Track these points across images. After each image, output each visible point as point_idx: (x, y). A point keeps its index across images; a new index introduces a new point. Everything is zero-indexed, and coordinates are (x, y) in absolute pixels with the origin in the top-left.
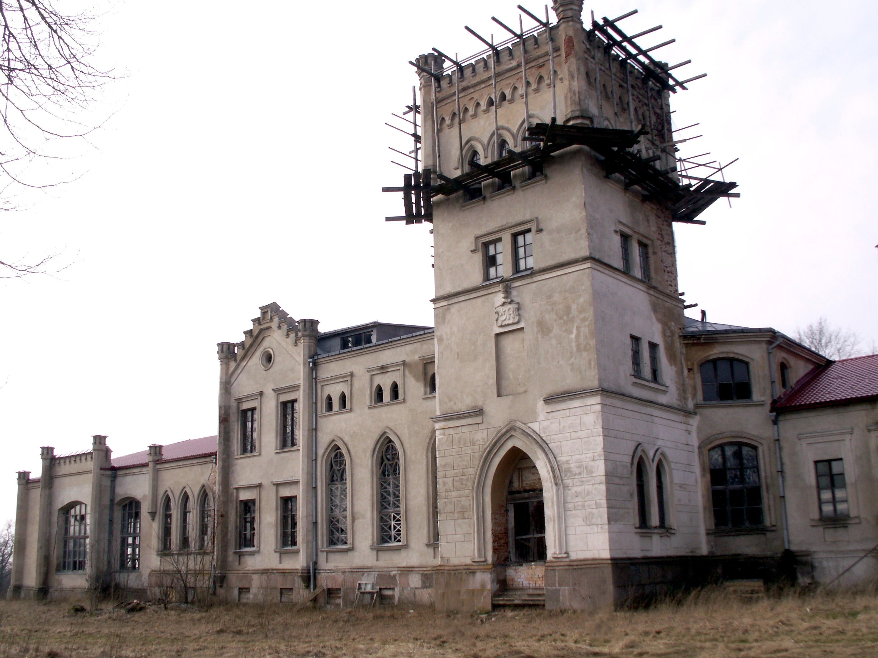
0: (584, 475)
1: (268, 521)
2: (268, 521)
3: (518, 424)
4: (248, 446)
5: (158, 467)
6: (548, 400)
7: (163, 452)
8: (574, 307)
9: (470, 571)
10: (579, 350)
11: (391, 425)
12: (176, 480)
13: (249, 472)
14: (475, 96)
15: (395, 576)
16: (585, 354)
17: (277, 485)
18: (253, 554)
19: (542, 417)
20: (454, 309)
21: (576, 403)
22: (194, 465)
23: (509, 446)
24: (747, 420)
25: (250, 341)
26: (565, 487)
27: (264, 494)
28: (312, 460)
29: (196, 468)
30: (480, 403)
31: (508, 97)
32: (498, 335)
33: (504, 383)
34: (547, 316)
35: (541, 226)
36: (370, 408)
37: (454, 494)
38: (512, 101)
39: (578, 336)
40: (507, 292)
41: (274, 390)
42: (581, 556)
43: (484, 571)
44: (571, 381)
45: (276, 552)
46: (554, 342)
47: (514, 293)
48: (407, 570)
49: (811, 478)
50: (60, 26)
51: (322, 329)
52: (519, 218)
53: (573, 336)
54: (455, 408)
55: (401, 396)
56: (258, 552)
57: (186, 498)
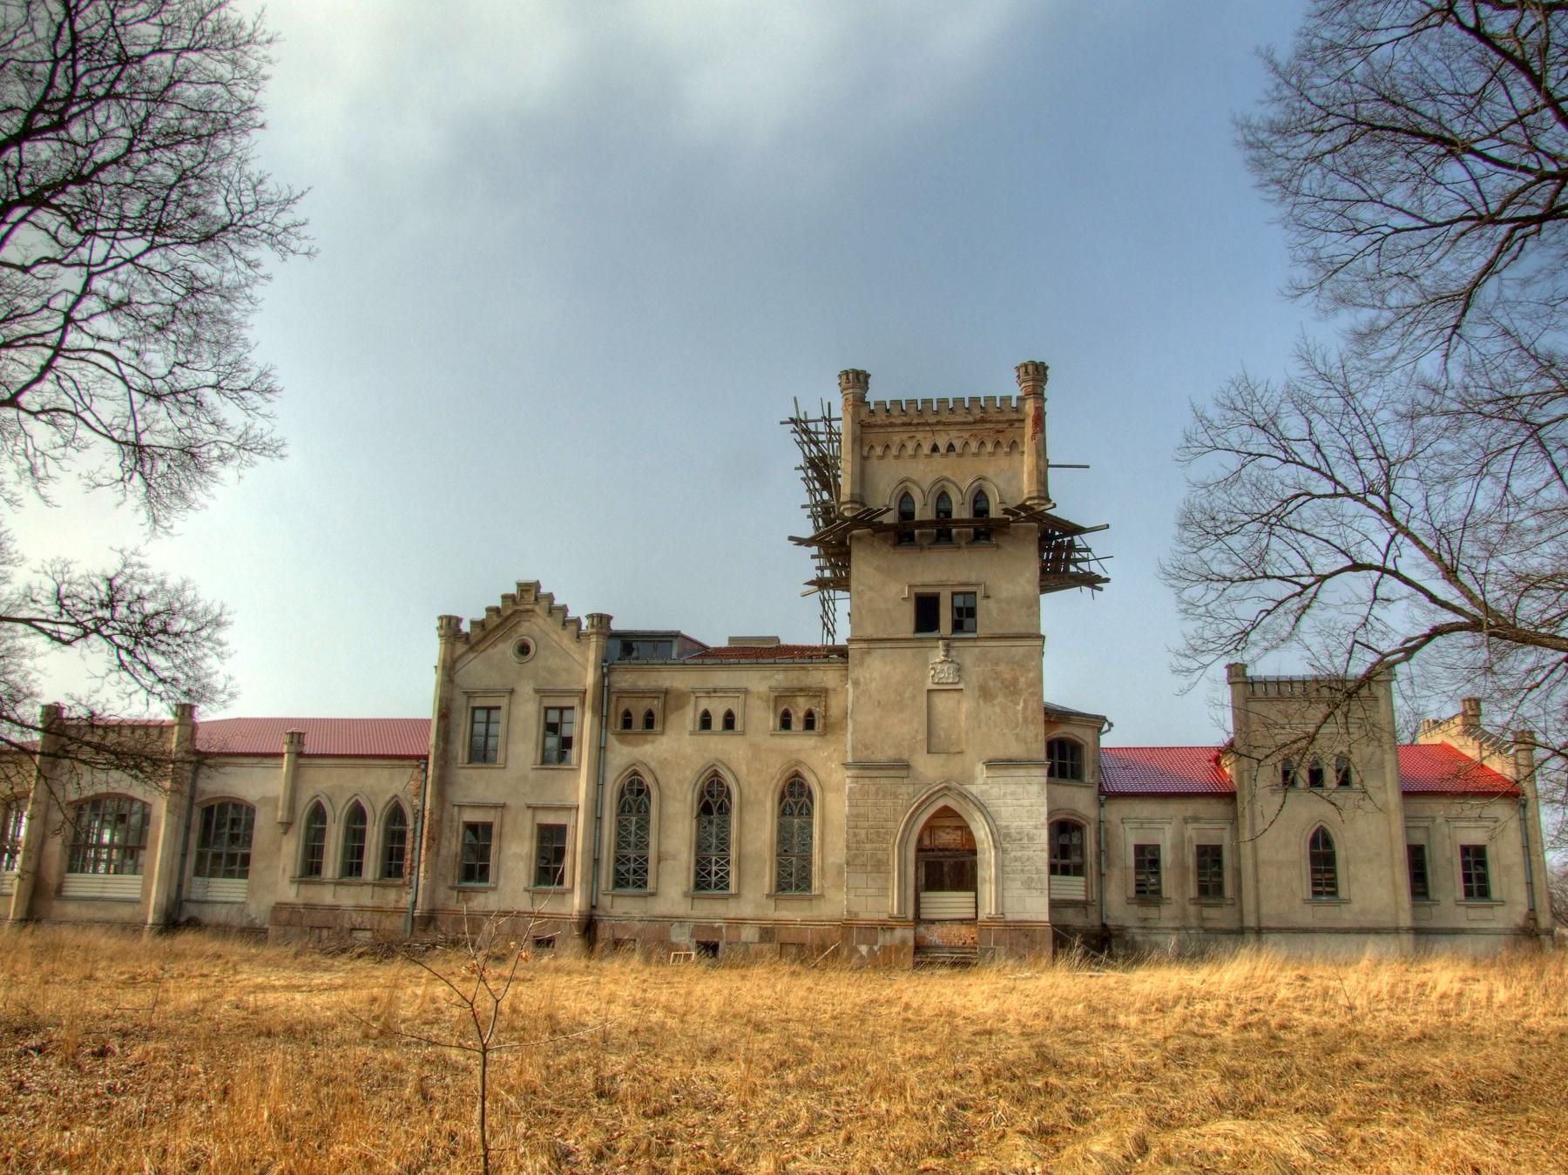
0: (1025, 840)
1: (515, 857)
2: (515, 857)
3: (954, 784)
4: (481, 754)
5: (302, 761)
6: (991, 764)
7: (199, 735)
8: (1022, 680)
9: (886, 927)
10: (1025, 719)
11: (720, 757)
12: (335, 787)
13: (477, 788)
14: (919, 436)
15: (720, 928)
16: (1032, 727)
17: (534, 808)
18: (485, 890)
19: (980, 781)
20: (877, 654)
21: (1021, 772)
22: (376, 766)
23: (940, 804)
24: (1080, 800)
25: (496, 620)
26: (1005, 851)
27: (508, 819)
28: (598, 782)
29: (379, 771)
30: (906, 756)
31: (958, 450)
32: (929, 691)
33: (934, 741)
34: (991, 683)
35: (989, 593)
36: (692, 734)
37: (868, 846)
38: (960, 455)
39: (1025, 708)
40: (948, 649)
41: (537, 691)
42: (1017, 918)
43: (905, 927)
44: (1015, 750)
45: (526, 890)
46: (998, 710)
47: (953, 653)
48: (739, 922)
49: (1131, 860)
50: (1000, 426)
51: (616, 626)
52: (962, 578)
53: (1020, 708)
54: (873, 757)
55: (738, 725)
56: (494, 889)
57: (357, 815)
